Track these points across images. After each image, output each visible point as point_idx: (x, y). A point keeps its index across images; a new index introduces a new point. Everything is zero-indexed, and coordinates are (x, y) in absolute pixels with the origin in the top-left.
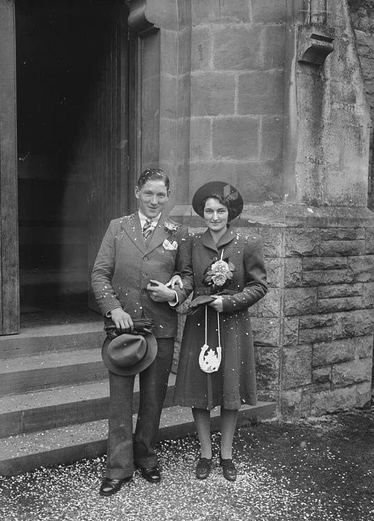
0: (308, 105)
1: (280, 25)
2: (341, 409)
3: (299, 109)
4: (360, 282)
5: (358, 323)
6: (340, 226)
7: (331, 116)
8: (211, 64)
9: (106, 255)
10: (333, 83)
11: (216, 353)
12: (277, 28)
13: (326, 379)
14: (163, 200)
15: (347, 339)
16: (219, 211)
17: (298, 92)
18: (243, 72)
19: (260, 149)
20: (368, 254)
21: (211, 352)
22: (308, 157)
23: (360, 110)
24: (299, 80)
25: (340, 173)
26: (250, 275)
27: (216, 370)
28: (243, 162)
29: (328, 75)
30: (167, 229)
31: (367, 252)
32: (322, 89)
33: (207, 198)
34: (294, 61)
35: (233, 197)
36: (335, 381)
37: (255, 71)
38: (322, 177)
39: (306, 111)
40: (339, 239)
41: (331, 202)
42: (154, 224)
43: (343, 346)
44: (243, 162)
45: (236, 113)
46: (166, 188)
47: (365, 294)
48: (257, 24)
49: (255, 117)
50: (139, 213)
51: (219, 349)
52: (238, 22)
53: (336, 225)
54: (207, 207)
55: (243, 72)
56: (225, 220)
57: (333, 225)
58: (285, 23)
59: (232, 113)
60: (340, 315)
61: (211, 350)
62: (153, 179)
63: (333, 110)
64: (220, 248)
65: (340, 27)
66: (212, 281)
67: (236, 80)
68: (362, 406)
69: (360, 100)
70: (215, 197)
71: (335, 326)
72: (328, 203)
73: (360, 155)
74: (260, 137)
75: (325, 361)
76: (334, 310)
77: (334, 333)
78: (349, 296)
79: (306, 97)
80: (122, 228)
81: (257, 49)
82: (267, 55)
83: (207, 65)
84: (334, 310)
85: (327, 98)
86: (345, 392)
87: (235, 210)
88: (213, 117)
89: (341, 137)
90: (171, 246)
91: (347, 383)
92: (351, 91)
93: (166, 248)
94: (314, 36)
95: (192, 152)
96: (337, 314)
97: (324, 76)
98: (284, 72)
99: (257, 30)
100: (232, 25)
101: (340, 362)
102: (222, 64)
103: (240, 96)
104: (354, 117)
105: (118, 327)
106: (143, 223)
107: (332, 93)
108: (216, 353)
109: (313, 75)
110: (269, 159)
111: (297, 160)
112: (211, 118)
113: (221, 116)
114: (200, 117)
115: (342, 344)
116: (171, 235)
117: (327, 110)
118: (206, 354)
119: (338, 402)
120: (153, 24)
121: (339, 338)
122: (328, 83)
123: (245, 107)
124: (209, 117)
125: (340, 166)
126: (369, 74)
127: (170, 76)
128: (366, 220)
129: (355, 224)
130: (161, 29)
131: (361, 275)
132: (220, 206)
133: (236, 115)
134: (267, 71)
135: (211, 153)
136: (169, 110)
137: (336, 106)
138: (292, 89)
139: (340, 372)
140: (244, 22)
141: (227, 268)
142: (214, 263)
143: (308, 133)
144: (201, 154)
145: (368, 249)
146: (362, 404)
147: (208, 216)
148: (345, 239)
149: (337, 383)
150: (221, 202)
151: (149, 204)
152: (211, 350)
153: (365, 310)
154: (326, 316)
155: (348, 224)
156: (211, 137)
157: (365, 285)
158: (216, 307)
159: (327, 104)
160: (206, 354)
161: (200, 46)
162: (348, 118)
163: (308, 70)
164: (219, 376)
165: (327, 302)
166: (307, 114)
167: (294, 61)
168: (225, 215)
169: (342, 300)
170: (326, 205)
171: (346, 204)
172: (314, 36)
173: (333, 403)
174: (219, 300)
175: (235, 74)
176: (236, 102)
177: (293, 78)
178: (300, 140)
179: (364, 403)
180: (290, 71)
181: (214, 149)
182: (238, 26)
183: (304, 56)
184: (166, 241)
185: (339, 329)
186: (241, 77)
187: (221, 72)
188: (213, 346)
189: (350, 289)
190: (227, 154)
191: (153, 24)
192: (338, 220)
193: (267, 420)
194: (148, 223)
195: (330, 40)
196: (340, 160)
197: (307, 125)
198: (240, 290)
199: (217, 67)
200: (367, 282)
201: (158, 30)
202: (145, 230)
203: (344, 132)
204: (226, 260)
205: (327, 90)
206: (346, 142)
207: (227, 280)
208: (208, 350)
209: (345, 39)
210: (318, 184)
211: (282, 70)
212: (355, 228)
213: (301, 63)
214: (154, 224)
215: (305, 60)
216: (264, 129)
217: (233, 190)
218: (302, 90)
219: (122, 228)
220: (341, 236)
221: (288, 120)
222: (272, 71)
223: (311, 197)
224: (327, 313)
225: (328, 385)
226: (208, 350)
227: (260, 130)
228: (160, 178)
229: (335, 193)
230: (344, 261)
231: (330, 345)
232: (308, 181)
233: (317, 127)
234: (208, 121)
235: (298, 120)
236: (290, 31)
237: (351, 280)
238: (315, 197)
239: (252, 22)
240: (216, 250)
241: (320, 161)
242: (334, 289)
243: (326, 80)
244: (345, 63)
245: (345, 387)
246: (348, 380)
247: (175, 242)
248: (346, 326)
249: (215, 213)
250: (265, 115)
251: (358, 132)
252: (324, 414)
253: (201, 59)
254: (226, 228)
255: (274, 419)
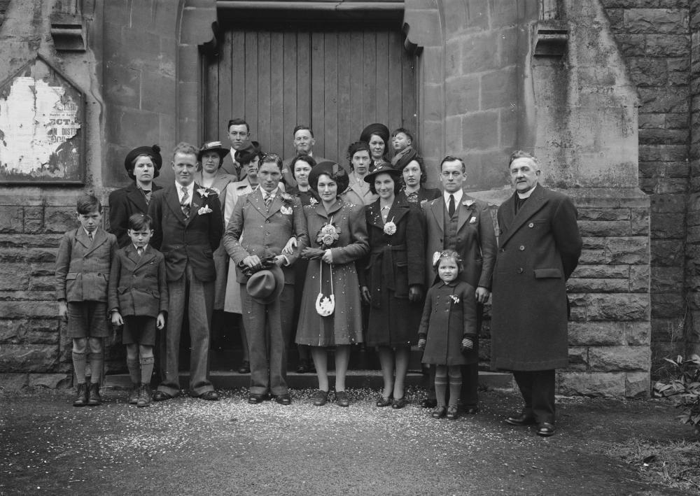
0: (549, 93)
1: (513, 27)
2: (599, 393)
3: (537, 98)
4: (624, 264)
5: (620, 305)
6: (591, 206)
7: (580, 101)
8: (461, 70)
9: (235, 222)
10: (582, 70)
11: (330, 300)
12: (511, 30)
13: (578, 359)
14: (191, 170)
15: (609, 321)
16: (330, 184)
17: (535, 83)
18: (485, 73)
19: (499, 138)
20: (636, 235)
21: (326, 299)
22: (551, 142)
23: (622, 91)
24: (536, 72)
25: (596, 155)
26: (354, 237)
27: (331, 313)
28: (487, 151)
29: (574, 61)
30: (283, 199)
31: (634, 233)
32: (566, 77)
33: (319, 175)
34: (528, 57)
35: (341, 174)
36: (592, 364)
37: (493, 71)
38: (571, 159)
39: (546, 99)
40: (590, 219)
41: (584, 183)
42: (273, 196)
43: (601, 328)
44: (487, 151)
45: (480, 109)
46: (278, 168)
47: (634, 277)
48: (495, 30)
49: (495, 111)
50: (176, 182)
51: (332, 297)
52: (480, 31)
53: (587, 205)
54: (320, 182)
55: (485, 73)
56: (334, 192)
57: (582, 206)
58: (516, 25)
59: (478, 109)
60: (594, 297)
61: (326, 298)
62: (267, 162)
63: (582, 95)
64: (330, 215)
65: (589, 16)
66: (322, 241)
67: (480, 81)
68: (632, 395)
69: (621, 80)
70: (326, 174)
71: (590, 307)
72: (580, 185)
73: (624, 133)
74: (499, 128)
75: (576, 341)
76: (588, 290)
77: (588, 314)
78: (608, 277)
79: (545, 86)
80: (248, 201)
81: (495, 51)
82: (504, 54)
83: (457, 71)
84: (588, 290)
85: (573, 85)
86: (608, 377)
87: (343, 184)
88: (462, 115)
89: (595, 119)
90: (287, 211)
91: (610, 368)
92: (607, 73)
93: (284, 213)
94: (541, 32)
95: (448, 147)
96: (592, 295)
97: (569, 64)
98: (516, 69)
99: (494, 35)
100: (476, 34)
101: (598, 345)
102: (469, 69)
103: (483, 94)
104: (613, 99)
105: (251, 266)
106: (264, 195)
107: (581, 78)
108: (330, 300)
109: (554, 66)
110: (507, 147)
111: (536, 145)
112: (461, 116)
113: (468, 114)
114: (453, 117)
115: (601, 327)
116: (288, 203)
117: (574, 96)
118: (321, 301)
119: (596, 386)
120: (416, 45)
121: (594, 319)
122: (573, 70)
123: (487, 103)
124: (459, 116)
125: (596, 147)
126: (677, 50)
127: (435, 85)
128: (630, 200)
129: (614, 205)
130: (425, 48)
131: (626, 256)
132: (331, 181)
133: (480, 111)
134: (503, 69)
135: (462, 146)
136: (433, 114)
137: (586, 90)
138: (527, 83)
139: (597, 355)
140: (485, 30)
141: (334, 231)
142: (324, 226)
143: (550, 120)
144: (454, 148)
145: (634, 230)
146: (633, 393)
147: (320, 188)
148: (598, 219)
149: (595, 366)
150: (331, 178)
151: (182, 174)
152: (326, 298)
153: (635, 294)
154: (575, 295)
155: (604, 204)
156: (462, 133)
157: (633, 267)
158: (327, 258)
159: (574, 90)
160: (321, 301)
161: (452, 56)
162: (604, 100)
163: (548, 62)
164: (330, 319)
165: (575, 281)
166: (548, 102)
167: (528, 57)
168: (335, 188)
169: (600, 281)
170: (577, 187)
171: (607, 185)
172: (541, 32)
173: (587, 385)
174: (329, 252)
175: (478, 75)
176: (480, 99)
177: (528, 71)
178: (539, 126)
179: (636, 393)
180: (523, 66)
181: (463, 143)
182: (480, 34)
183: (537, 50)
184: (283, 208)
185: (594, 310)
186: (483, 77)
187: (468, 75)
188: (327, 294)
189: (610, 271)
190: (474, 146)
191: (416, 45)
192: (588, 200)
193: (501, 389)
194: (268, 195)
195: (565, 32)
196: (595, 142)
197: (547, 112)
198: (346, 246)
199: (465, 71)
200: (636, 264)
201: (422, 49)
202: (265, 200)
203: (600, 115)
204: (333, 224)
205: (574, 76)
206: (602, 124)
207: (335, 240)
208: (323, 298)
209: (595, 26)
210: (565, 167)
211: (514, 66)
212: (614, 208)
213: (537, 56)
214: (273, 196)
215: (539, 53)
216: (503, 120)
217: (340, 168)
218: (540, 83)
219: (248, 201)
220: (595, 216)
221: (524, 110)
222: (507, 68)
223: (556, 180)
224: (576, 293)
225: (583, 367)
226: (323, 298)
227: (499, 122)
228: (273, 160)
229: (591, 175)
230: (600, 241)
231: (583, 325)
232: (552, 164)
233: (561, 111)
234: (459, 119)
235: (536, 109)
236: (523, 30)
237: (610, 260)
238: (562, 179)
239: (490, 30)
240: (326, 216)
241: (568, 145)
242: (585, 269)
243: (570, 67)
244: (598, 49)
245: (607, 372)
246: (610, 364)
247: (290, 208)
248: (603, 308)
249: (326, 186)
250: (503, 108)
251: (621, 114)
252: (575, 395)
253: (453, 67)
254: (335, 200)
255: (510, 390)
